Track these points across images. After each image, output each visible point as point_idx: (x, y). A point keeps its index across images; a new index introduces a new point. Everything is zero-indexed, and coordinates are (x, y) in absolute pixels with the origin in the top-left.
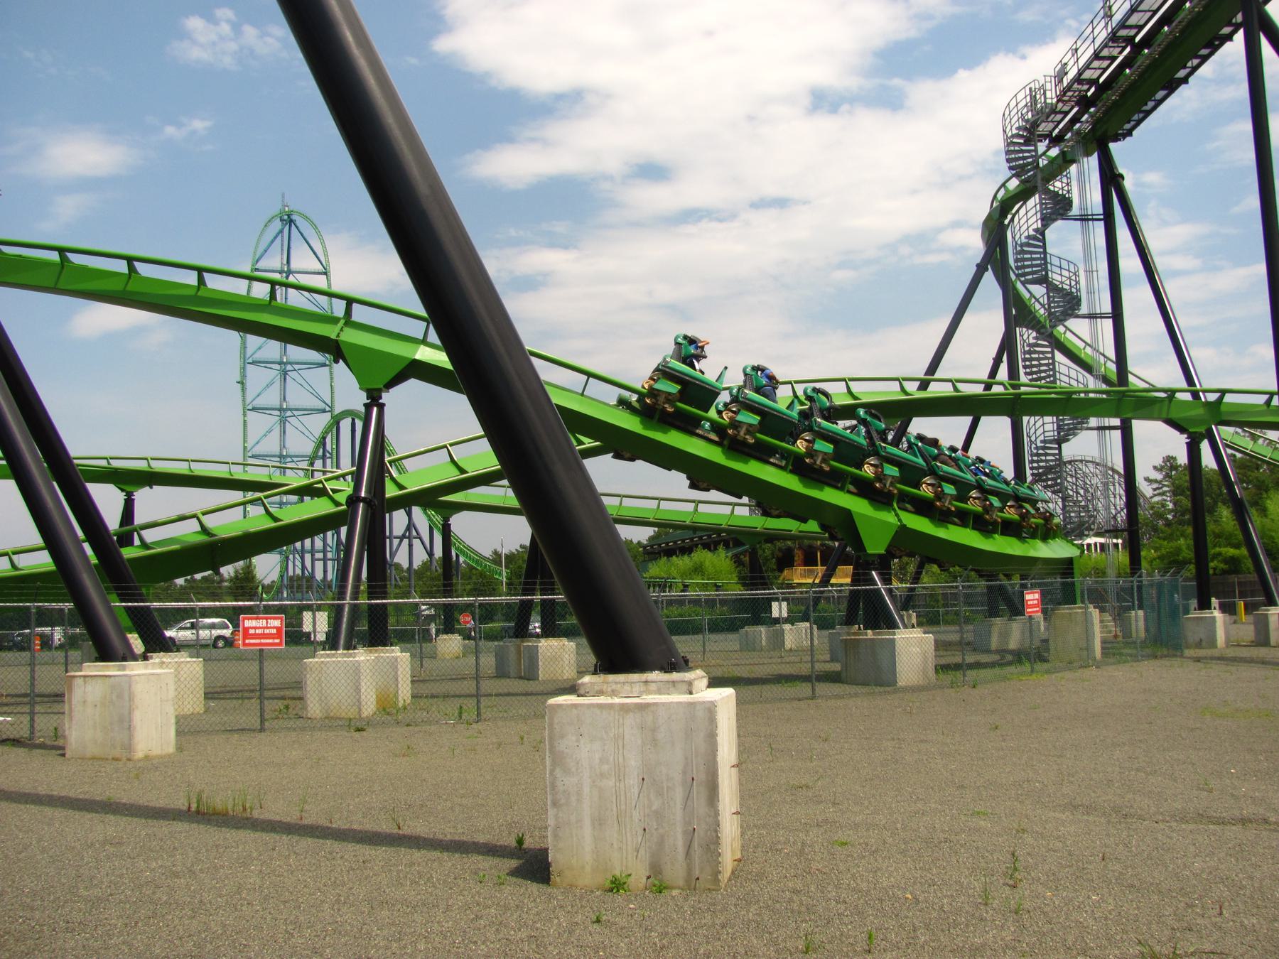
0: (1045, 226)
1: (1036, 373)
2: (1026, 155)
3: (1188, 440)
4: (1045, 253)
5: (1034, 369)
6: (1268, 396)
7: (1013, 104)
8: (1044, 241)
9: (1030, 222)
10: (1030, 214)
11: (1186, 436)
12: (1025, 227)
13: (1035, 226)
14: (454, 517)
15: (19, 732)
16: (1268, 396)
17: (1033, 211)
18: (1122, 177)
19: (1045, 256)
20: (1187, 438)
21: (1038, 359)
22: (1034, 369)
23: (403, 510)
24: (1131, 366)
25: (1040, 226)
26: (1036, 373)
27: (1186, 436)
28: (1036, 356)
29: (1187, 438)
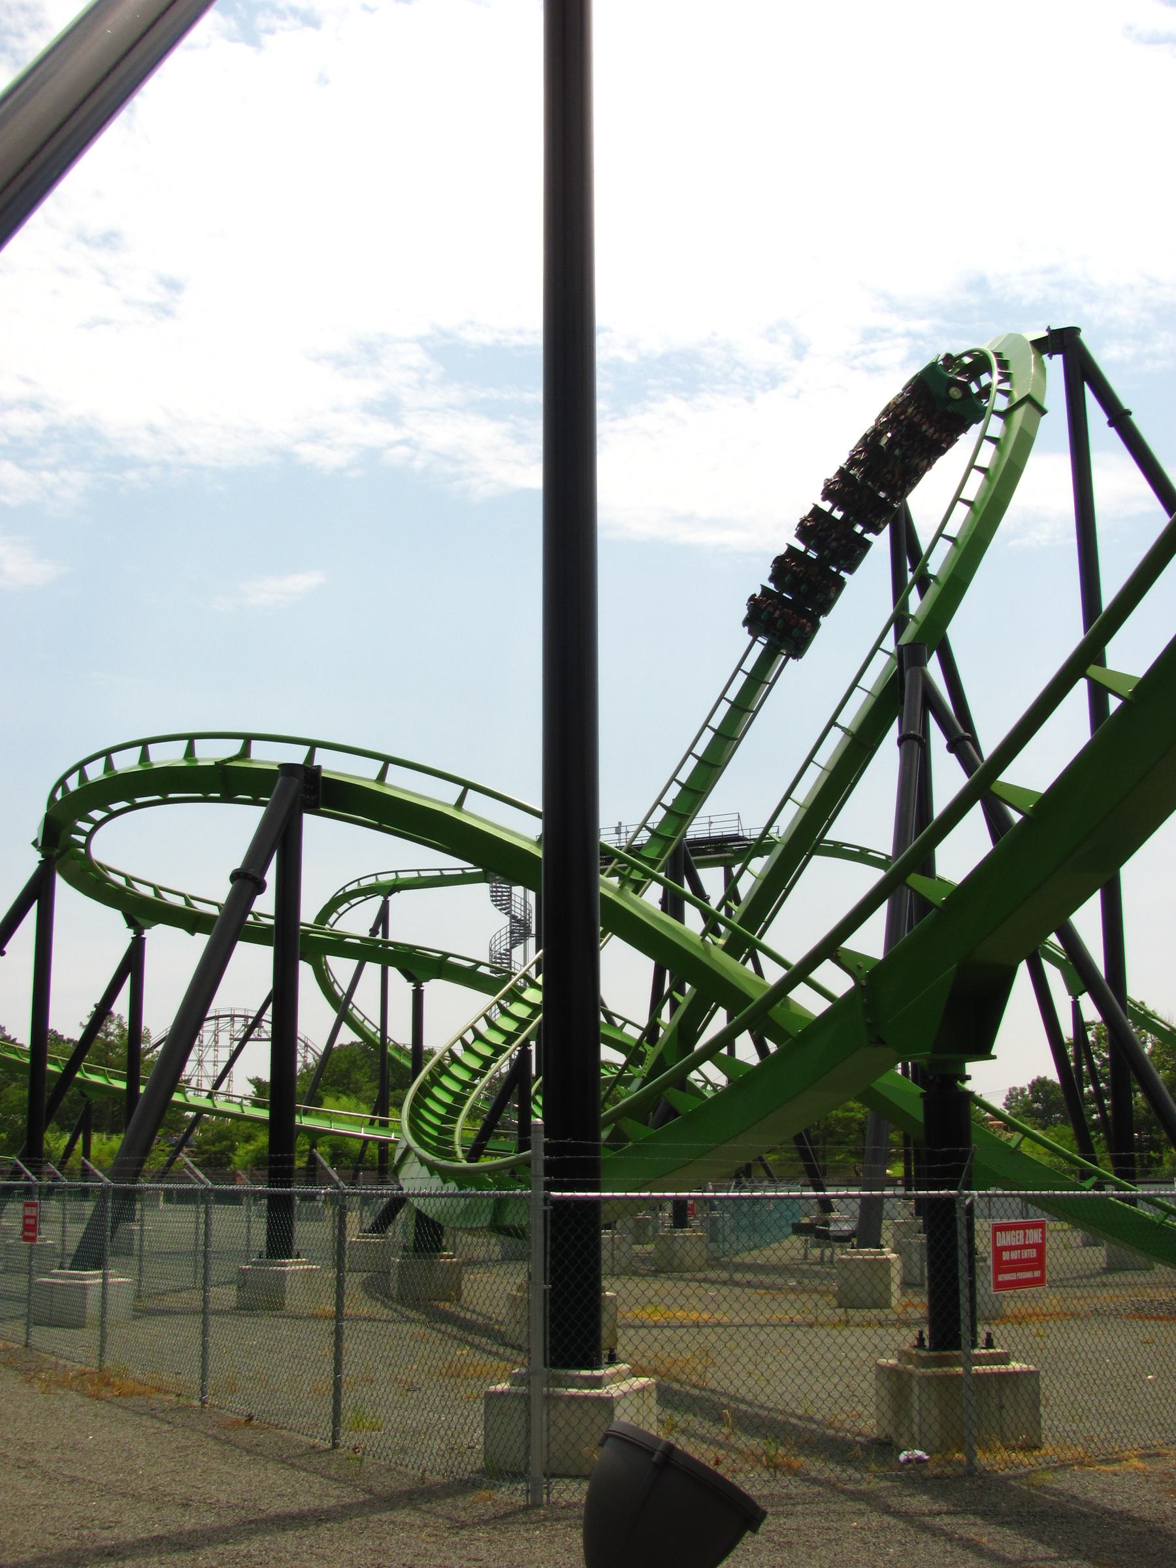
0: (512, 948)
1: (499, 901)
2: (504, 890)
3: (414, 988)
4: (510, 959)
5: (499, 898)
6: (103, 759)
7: (498, 936)
8: (510, 955)
9: (502, 944)
10: (502, 939)
11: (413, 984)
12: (498, 947)
13: (505, 947)
14: (433, 981)
15: (774, 1299)
16: (103, 759)
17: (504, 937)
18: (1129, 413)
19: (511, 962)
20: (414, 986)
21: (502, 892)
22: (499, 898)
23: (393, 937)
24: (389, 1034)
25: (508, 948)
26: (499, 901)
27: (413, 984)
28: (500, 890)
29: (414, 986)
